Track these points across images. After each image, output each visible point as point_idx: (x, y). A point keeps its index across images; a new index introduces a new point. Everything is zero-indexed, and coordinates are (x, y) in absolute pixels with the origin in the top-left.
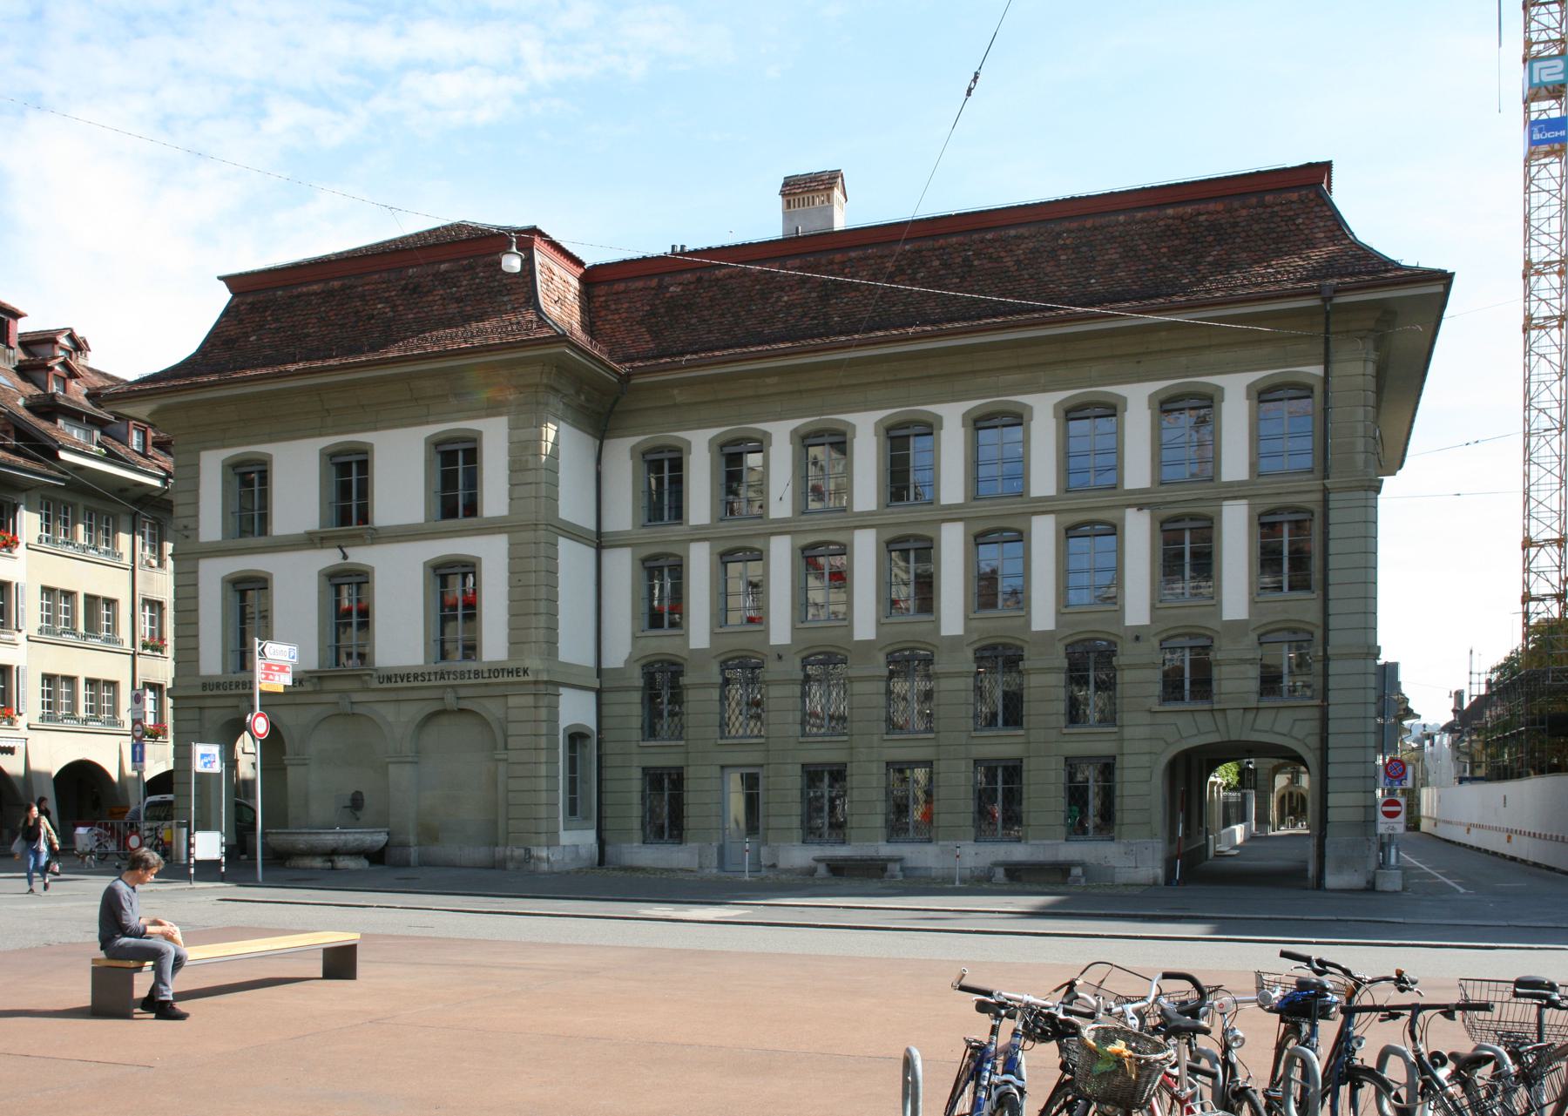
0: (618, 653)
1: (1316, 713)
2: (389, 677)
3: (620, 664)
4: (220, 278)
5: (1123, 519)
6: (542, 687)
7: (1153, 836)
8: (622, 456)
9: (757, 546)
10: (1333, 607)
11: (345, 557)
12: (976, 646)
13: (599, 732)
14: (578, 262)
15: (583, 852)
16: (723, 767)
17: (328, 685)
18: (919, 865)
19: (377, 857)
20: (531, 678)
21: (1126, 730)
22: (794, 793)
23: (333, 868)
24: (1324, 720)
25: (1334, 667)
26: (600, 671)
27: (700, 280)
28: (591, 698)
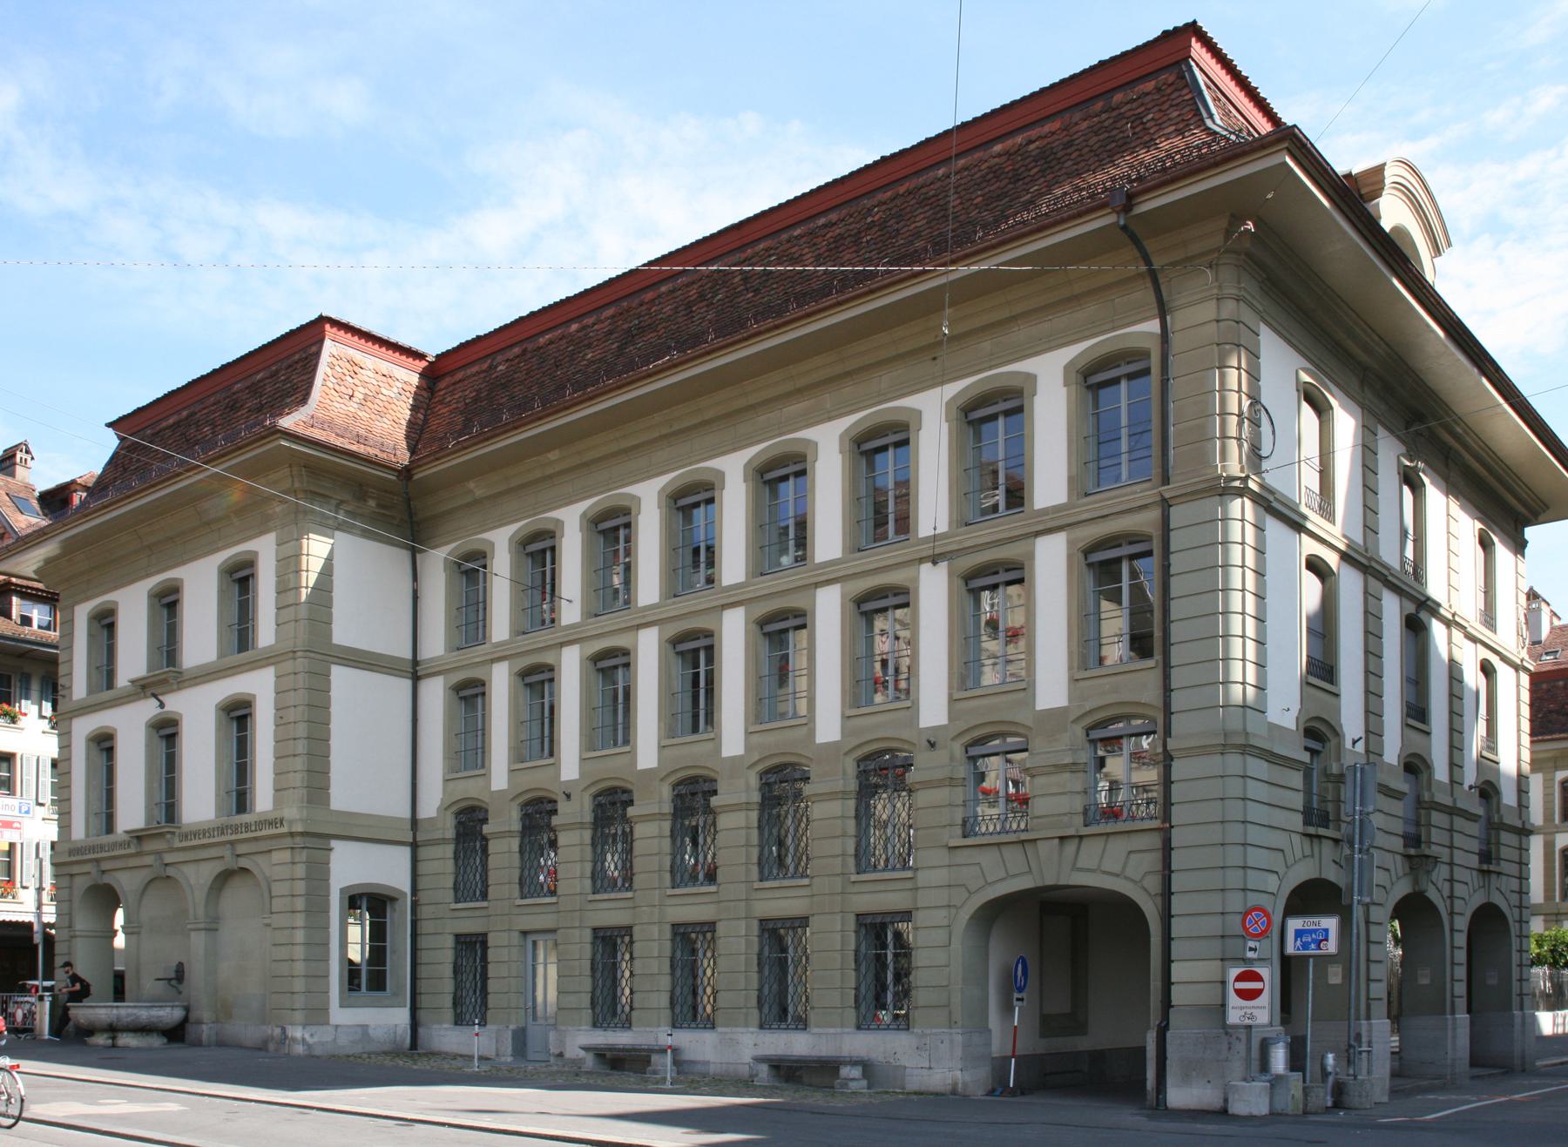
0: (430, 807)
1: (1155, 841)
2: (195, 834)
3: (433, 813)
4: (109, 425)
5: (916, 580)
6: (298, 839)
7: (951, 1024)
8: (436, 561)
11: (162, 705)
12: (760, 767)
14: (419, 356)
15: (399, 1031)
16: (525, 933)
18: (699, 1058)
19: (176, 1034)
20: (284, 830)
21: (920, 874)
22: (448, 956)
23: (114, 1046)
24: (1167, 849)
25: (1179, 769)
26: (414, 822)
27: (524, 352)
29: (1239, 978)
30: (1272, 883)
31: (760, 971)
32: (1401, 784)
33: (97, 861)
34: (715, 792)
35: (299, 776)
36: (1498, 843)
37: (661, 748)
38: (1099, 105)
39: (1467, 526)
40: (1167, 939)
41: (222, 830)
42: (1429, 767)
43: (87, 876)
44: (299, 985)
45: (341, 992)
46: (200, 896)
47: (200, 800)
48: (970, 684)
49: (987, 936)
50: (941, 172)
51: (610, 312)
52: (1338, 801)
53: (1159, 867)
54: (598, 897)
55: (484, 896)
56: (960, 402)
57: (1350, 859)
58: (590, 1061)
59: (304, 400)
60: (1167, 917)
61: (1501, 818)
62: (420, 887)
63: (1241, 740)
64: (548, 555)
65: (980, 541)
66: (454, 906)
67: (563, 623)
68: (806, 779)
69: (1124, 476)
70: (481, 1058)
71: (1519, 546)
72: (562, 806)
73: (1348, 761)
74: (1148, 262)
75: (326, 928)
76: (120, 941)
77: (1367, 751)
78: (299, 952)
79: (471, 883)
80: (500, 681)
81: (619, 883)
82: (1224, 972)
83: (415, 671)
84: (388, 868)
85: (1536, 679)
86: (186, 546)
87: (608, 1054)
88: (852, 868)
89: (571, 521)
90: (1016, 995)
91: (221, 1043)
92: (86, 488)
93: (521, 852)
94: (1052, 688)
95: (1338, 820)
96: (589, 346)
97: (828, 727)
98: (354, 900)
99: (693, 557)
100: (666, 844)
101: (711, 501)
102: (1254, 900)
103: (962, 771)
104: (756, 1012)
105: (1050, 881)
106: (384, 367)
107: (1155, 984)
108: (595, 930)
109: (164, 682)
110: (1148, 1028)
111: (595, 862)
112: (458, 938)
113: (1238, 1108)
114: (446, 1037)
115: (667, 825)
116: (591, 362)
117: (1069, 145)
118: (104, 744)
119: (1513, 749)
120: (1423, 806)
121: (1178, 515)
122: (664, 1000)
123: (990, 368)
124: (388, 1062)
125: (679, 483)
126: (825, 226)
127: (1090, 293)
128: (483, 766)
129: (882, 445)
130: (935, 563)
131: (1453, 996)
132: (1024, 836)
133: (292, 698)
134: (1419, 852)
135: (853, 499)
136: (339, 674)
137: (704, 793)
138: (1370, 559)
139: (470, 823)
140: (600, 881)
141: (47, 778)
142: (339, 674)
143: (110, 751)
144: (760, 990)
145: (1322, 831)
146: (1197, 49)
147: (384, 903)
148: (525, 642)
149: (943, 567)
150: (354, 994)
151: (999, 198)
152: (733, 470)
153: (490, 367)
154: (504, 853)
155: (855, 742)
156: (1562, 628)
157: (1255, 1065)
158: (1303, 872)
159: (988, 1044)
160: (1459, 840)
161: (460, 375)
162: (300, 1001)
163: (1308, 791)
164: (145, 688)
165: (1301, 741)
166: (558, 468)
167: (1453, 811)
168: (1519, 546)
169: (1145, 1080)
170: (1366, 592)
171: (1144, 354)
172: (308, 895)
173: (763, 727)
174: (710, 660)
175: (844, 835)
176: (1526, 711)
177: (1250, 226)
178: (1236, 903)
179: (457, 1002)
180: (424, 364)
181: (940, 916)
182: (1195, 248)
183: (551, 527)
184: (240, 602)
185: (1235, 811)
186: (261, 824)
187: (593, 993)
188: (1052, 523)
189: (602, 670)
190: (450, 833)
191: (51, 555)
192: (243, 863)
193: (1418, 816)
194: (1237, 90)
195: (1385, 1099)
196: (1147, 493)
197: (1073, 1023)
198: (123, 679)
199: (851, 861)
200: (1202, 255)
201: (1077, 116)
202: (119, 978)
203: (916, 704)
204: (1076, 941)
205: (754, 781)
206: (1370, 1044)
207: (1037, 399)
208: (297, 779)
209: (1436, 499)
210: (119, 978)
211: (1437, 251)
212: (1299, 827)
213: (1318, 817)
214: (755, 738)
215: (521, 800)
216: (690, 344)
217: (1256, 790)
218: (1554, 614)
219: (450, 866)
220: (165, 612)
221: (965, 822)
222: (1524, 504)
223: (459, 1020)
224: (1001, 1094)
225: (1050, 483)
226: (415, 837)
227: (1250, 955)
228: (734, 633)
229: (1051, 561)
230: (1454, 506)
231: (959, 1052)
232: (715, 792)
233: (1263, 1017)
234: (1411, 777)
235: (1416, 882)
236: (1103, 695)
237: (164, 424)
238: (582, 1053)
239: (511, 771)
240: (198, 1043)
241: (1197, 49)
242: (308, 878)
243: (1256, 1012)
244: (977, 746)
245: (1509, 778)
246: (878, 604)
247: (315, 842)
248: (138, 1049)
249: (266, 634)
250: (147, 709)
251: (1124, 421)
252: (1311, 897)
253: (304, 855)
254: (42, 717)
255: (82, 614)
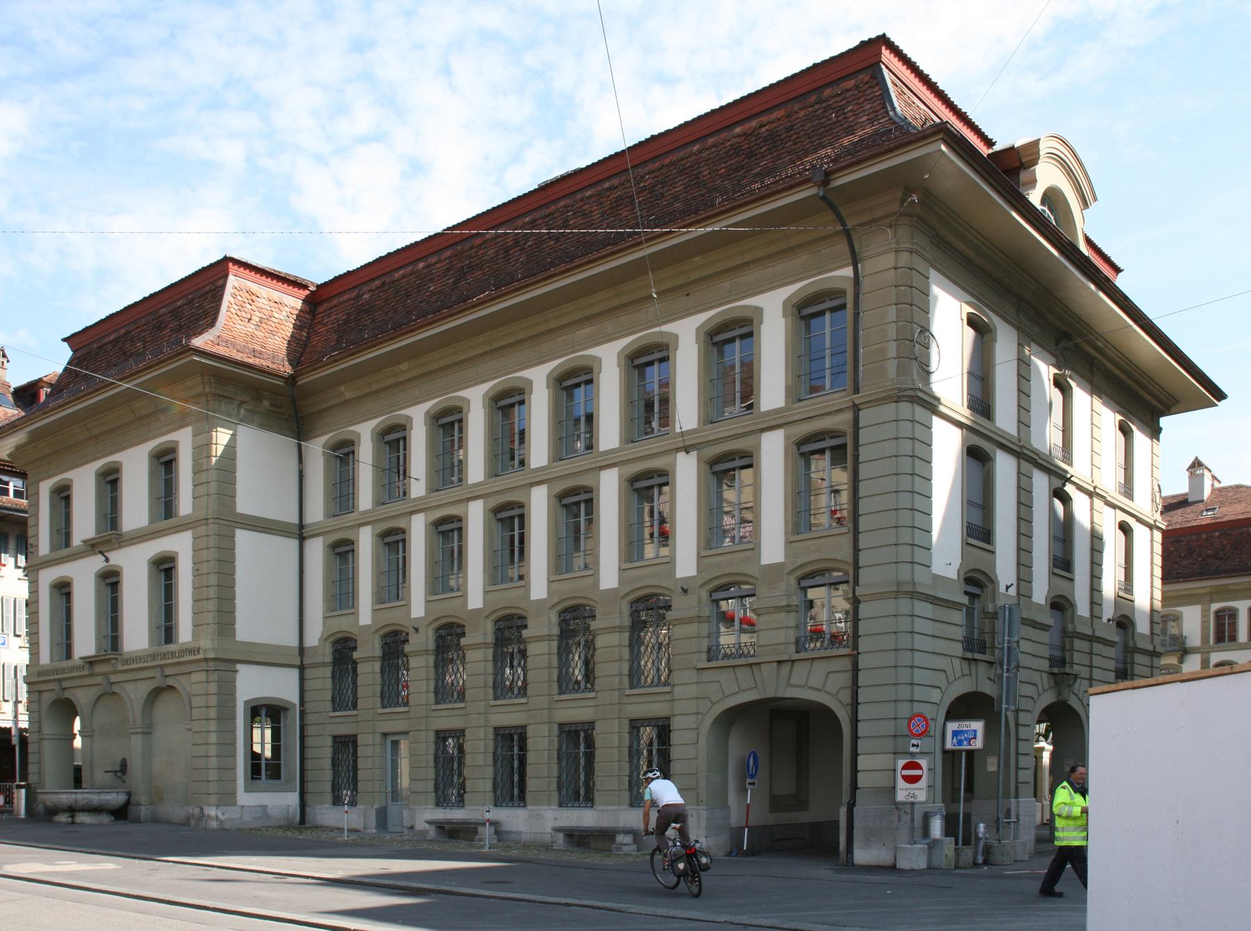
0: (314, 636)
1: (847, 664)
3: (316, 643)
4: (64, 340)
5: (674, 465)
8: (316, 449)
9: (402, 525)
10: (864, 542)
11: (107, 560)
12: (559, 608)
13: (302, 702)
15: (291, 810)
16: (385, 735)
17: (99, 669)
18: (513, 829)
19: (120, 813)
20: (200, 656)
21: (676, 690)
22: (328, 753)
23: (73, 823)
24: (855, 670)
25: (864, 610)
26: (302, 649)
27: (383, 284)
28: (293, 675)
29: (905, 767)
30: (935, 695)
31: (559, 763)
32: (1047, 618)
33: (59, 680)
34: (526, 627)
35: (211, 615)
36: (1133, 663)
37: (486, 593)
38: (813, 98)
39: (1109, 418)
40: (855, 738)
41: (154, 656)
42: (1072, 605)
43: (53, 692)
44: (213, 775)
45: (246, 780)
46: (138, 706)
47: (137, 633)
48: (713, 544)
49: (727, 737)
50: (696, 148)
51: (448, 253)
52: (993, 633)
53: (849, 683)
54: (439, 707)
55: (355, 706)
56: (555, 374)
57: (1001, 677)
58: (432, 831)
59: (212, 324)
60: (855, 721)
61: (1135, 643)
62: (306, 699)
63: (909, 588)
64: (401, 443)
65: (720, 436)
66: (332, 714)
67: (413, 496)
68: (668, 608)
69: (828, 386)
70: (351, 831)
71: (1154, 432)
72: (413, 638)
73: (1000, 602)
74: (843, 223)
75: (234, 731)
76: (78, 743)
77: (1018, 594)
78: (213, 750)
79: (344, 698)
80: (366, 541)
81: (582, 685)
82: (895, 764)
83: (301, 533)
84: (281, 685)
85: (1166, 534)
86: (123, 436)
87: (447, 827)
88: (627, 686)
89: (418, 416)
90: (748, 781)
91: (155, 820)
92: (50, 385)
93: (382, 672)
94: (773, 546)
95: (993, 647)
96: (432, 280)
97: (475, 600)
98: (256, 711)
99: (508, 445)
100: (490, 667)
101: (664, 360)
102: (918, 708)
103: (706, 611)
104: (556, 794)
105: (770, 694)
106: (276, 295)
107: (846, 771)
108: (561, 725)
109: (109, 541)
110: (842, 805)
111: (437, 680)
112: (336, 738)
113: (902, 864)
114: (326, 814)
115: (490, 652)
116: (433, 293)
117: (790, 129)
118: (63, 590)
119: (1147, 592)
120: (1068, 635)
121: (865, 417)
122: (489, 785)
123: (729, 302)
124: (280, 833)
125: (500, 388)
126: (609, 189)
127: (800, 246)
128: (353, 606)
129: (648, 361)
130: (687, 452)
131: (1017, 782)
132: (751, 660)
133: (205, 555)
134: (1062, 670)
135: (628, 403)
136: (243, 538)
137: (518, 627)
138: (1021, 447)
139: (343, 650)
140: (565, 683)
141: (22, 616)
142: (243, 538)
143: (68, 596)
144: (559, 777)
145: (977, 656)
146: (886, 55)
147: (279, 712)
148: (384, 511)
149: (694, 455)
150: (257, 782)
151: (737, 170)
152: (609, 358)
153: (357, 296)
154: (369, 674)
155: (630, 588)
156: (1220, 490)
157: (918, 833)
158: (962, 687)
159: (728, 817)
160: (1097, 661)
161: (334, 302)
162: (213, 788)
163: (970, 626)
164: (93, 547)
165: (963, 587)
166: (408, 376)
167: (1092, 639)
168: (1154, 432)
169: (838, 843)
170: (1019, 473)
171: (841, 293)
172: (219, 706)
173: (709, 552)
174: (522, 526)
175: (620, 660)
176: (1158, 560)
177: (915, 198)
178: (905, 710)
179: (336, 788)
180: (307, 292)
181: (691, 721)
182: (879, 213)
183: (402, 422)
184: (166, 481)
185: (905, 641)
186: (183, 652)
187: (436, 780)
188: (774, 422)
189: (442, 533)
190: (329, 658)
191: (21, 442)
192: (170, 682)
193: (1064, 644)
194: (920, 85)
195: (1026, 858)
196: (841, 399)
197: (798, 801)
198: (77, 540)
199: (626, 680)
200: (886, 217)
201: (796, 107)
202: (78, 770)
203: (597, 572)
204: (794, 739)
205: (554, 617)
206: (1017, 816)
207: (533, 396)
208: (210, 617)
209: (1081, 398)
210: (78, 770)
211: (1085, 204)
212: (960, 652)
213: (977, 646)
214: (556, 586)
215: (381, 632)
216: (505, 283)
217: (920, 625)
218: (1214, 478)
219: (329, 683)
220: (109, 487)
221: (709, 650)
222: (1159, 401)
223: (337, 801)
224: (736, 855)
225: (773, 390)
226: (301, 660)
227: (913, 750)
228: (539, 504)
229: (773, 450)
230: (1098, 403)
231: (703, 824)
232: (526, 627)
233: (922, 796)
234: (1056, 612)
235: (1059, 694)
236: (811, 553)
237: (106, 340)
238: (427, 826)
239: (374, 610)
240: (137, 821)
241: (886, 55)
242: (219, 694)
243: (917, 793)
244: (721, 589)
245: (1142, 612)
246: (647, 486)
247: (224, 666)
248: (91, 825)
249: (185, 505)
250: (95, 563)
251: (828, 344)
252: (965, 707)
253: (215, 676)
254: (17, 567)
255: (45, 488)
